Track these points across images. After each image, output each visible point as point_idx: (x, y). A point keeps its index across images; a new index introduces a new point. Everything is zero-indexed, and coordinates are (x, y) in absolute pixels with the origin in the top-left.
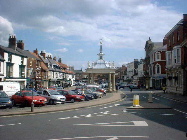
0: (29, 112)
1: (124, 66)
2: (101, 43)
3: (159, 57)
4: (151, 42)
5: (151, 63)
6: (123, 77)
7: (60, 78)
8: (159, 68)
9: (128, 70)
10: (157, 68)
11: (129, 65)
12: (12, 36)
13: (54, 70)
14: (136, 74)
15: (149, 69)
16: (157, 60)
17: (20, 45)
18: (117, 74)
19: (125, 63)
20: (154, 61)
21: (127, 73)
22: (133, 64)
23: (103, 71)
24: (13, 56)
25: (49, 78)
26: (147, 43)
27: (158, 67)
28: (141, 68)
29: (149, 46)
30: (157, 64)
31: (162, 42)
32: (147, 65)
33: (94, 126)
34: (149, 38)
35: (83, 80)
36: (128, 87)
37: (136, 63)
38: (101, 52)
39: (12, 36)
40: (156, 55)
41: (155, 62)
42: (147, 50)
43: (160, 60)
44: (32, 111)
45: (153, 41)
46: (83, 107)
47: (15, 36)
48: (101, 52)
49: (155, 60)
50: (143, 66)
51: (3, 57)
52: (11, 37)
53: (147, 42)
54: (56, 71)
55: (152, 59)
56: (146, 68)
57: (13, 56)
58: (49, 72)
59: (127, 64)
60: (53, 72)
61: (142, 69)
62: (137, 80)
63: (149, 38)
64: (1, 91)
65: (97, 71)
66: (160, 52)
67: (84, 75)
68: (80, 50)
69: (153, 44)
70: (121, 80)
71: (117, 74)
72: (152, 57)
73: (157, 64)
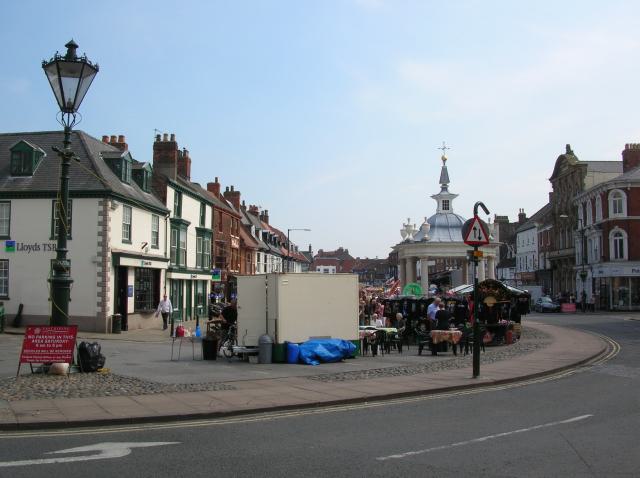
0: (468, 383)
2: (444, 160)
3: (620, 207)
4: (576, 158)
8: (621, 241)
12: (166, 135)
16: (612, 216)
17: (183, 163)
24: (186, 198)
26: (561, 161)
27: (618, 238)
29: (568, 172)
30: (617, 229)
31: (620, 159)
34: (568, 147)
36: (38, 373)
38: (444, 188)
39: (166, 135)
40: (611, 199)
41: (609, 222)
43: (624, 215)
44: (476, 372)
45: (582, 155)
46: (580, 363)
47: (173, 136)
48: (444, 188)
49: (606, 214)
51: (164, 200)
52: (162, 139)
56: (547, 244)
63: (568, 147)
66: (625, 190)
69: (586, 165)
73: (617, 229)
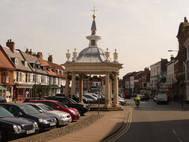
1: (147, 70)
2: (94, 17)
6: (145, 85)
7: (42, 84)
9: (152, 74)
11: (153, 68)
13: (29, 70)
14: (164, 80)
18: (137, 81)
19: (148, 66)
21: (151, 79)
22: (159, 65)
23: (99, 68)
25: (16, 82)
28: (171, 70)
34: (185, 18)
35: (92, 89)
37: (164, 63)
38: (93, 33)
42: (180, 40)
48: (93, 33)
54: (32, 72)
57: (35, 71)
58: (15, 73)
59: (151, 66)
60: (23, 74)
61: (173, 72)
63: (185, 18)
65: (87, 68)
67: (93, 82)
70: (143, 89)
71: (137, 81)
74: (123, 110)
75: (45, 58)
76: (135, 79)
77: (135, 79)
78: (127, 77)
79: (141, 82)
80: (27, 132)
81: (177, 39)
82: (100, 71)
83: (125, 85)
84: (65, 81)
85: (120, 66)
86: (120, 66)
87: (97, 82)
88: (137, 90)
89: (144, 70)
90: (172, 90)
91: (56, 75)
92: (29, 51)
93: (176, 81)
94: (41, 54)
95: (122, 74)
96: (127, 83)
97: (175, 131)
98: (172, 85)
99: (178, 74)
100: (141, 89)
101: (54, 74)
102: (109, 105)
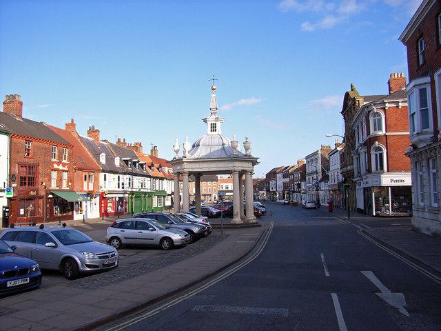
2: (246, 138)
5: (357, 145)
6: (299, 186)
7: (142, 190)
8: (381, 155)
10: (376, 155)
11: (309, 160)
15: (355, 162)
18: (287, 180)
20: (366, 137)
27: (378, 152)
32: (349, 153)
33: (227, 277)
40: (371, 119)
41: (370, 139)
50: (339, 158)
53: (347, 95)
55: (361, 134)
61: (338, 166)
62: (328, 192)
64: (334, 296)
68: (289, 131)
71: (287, 180)
72: (360, 129)
74: (260, 226)
75: (146, 151)
76: (284, 177)
77: (284, 177)
78: (272, 175)
79: (292, 181)
80: (8, 283)
81: (342, 117)
82: (224, 169)
83: (269, 186)
84: (173, 182)
85: (254, 162)
86: (254, 162)
87: (227, 184)
88: (287, 193)
89: (265, 177)
90: (338, 193)
91: (163, 176)
92: (122, 141)
93: (341, 178)
94: (140, 145)
95: (260, 173)
96: (272, 183)
97: (324, 256)
98: (338, 184)
99: (345, 169)
100: (294, 192)
101: (161, 175)
102: (237, 220)
